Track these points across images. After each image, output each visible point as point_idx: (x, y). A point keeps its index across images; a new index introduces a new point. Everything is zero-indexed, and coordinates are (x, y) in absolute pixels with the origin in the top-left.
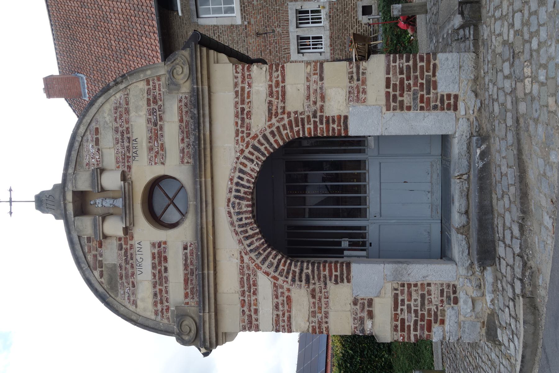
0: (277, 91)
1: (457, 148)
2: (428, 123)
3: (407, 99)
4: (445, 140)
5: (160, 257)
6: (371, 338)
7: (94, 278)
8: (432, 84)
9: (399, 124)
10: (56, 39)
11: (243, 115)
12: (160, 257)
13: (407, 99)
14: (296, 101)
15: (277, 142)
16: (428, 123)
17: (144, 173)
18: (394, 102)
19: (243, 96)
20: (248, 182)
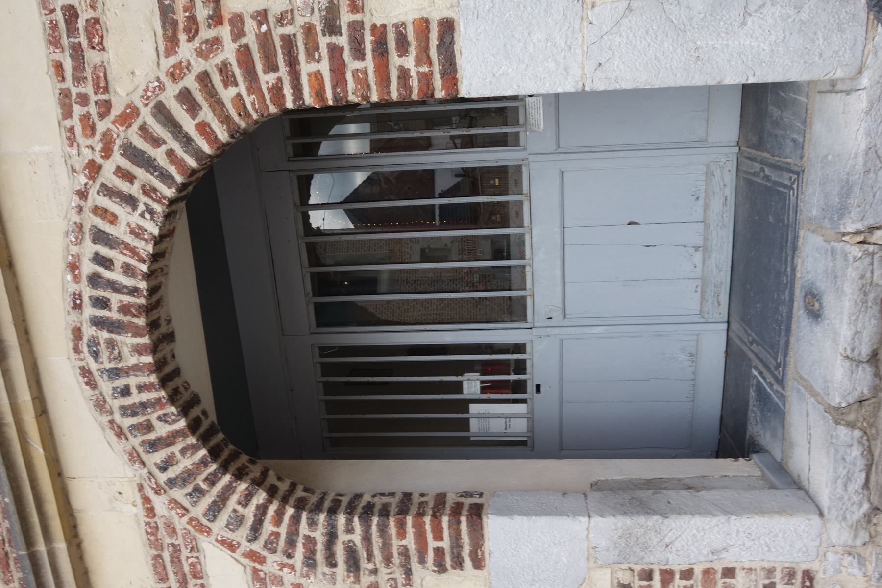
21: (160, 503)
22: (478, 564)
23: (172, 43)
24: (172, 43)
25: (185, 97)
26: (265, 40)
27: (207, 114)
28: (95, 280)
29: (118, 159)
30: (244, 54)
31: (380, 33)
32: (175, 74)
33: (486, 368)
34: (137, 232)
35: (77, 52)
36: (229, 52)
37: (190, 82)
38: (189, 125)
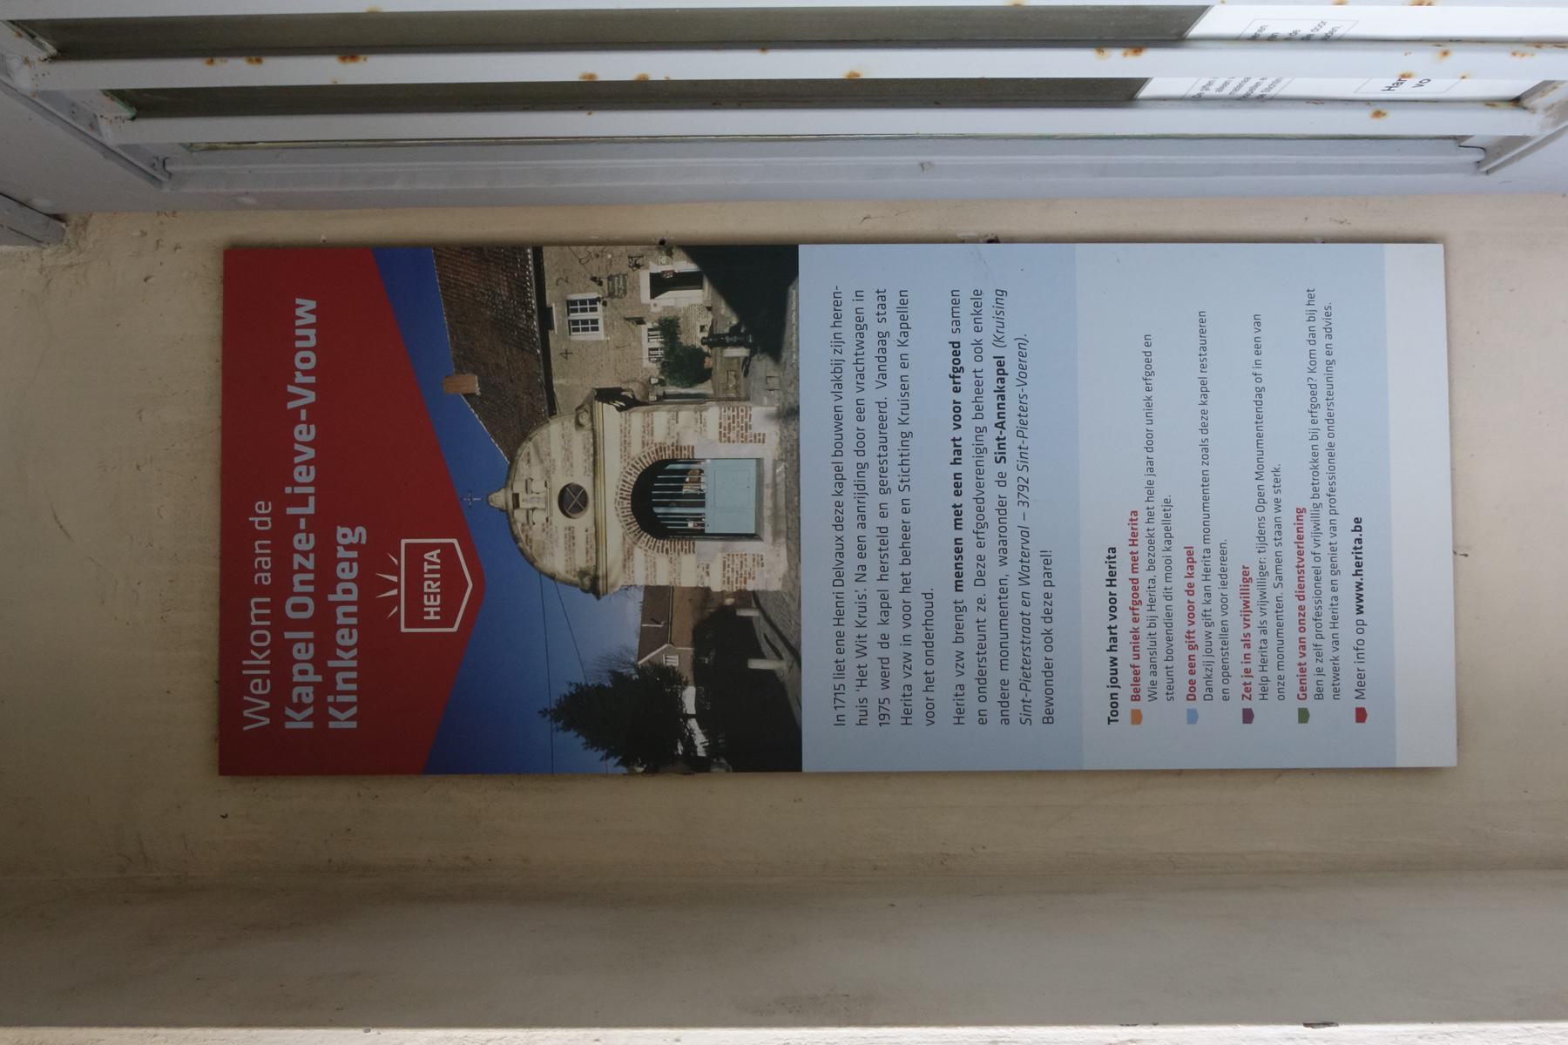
0: (648, 429)
1: (768, 465)
2: (748, 450)
3: (733, 435)
4: (759, 461)
5: (571, 535)
6: (708, 589)
7: (1459, 57)
8: (748, 427)
9: (725, 450)
10: (225, 17)
11: (626, 444)
12: (571, 535)
13: (733, 435)
14: (659, 436)
15: (648, 462)
16: (748, 450)
17: (559, 482)
18: (724, 437)
19: (625, 433)
20: (629, 488)
33: (681, 496)
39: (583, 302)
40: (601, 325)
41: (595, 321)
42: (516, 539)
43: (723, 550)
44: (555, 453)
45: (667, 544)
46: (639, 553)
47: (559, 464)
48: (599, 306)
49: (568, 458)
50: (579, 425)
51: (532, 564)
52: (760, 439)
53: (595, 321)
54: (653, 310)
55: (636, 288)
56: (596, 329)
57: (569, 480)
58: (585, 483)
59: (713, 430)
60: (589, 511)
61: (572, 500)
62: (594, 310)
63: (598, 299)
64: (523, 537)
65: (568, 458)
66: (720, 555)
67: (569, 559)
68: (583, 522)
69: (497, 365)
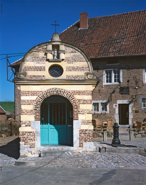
0: (85, 102)
8: (86, 141)
11: (79, 93)
13: (83, 135)
14: (82, 107)
15: (72, 102)
17: (63, 65)
19: (83, 93)
20: (61, 94)
21: (41, 93)
22: (35, 120)
23: (78, 100)
24: (78, 100)
25: (74, 100)
26: (78, 107)
27: (73, 102)
28: (61, 91)
29: (70, 94)
30: (77, 105)
31: (78, 115)
32: (76, 100)
34: (65, 95)
35: (78, 93)
36: (77, 104)
37: (75, 101)
38: (72, 100)
39: (119, 76)
40: (109, 84)
41: (110, 82)
42: (39, 45)
43: (37, 132)
44: (74, 63)
45: (39, 109)
46: (34, 98)
47: (71, 65)
48: (117, 83)
49: (74, 69)
50: (87, 74)
51: (29, 52)
52: (81, 145)
53: (110, 82)
54: (114, 105)
55: (123, 98)
56: (107, 82)
57: (65, 69)
58: (64, 76)
59: (85, 127)
60: (52, 78)
61: (56, 70)
62: (115, 81)
63: (120, 83)
64: (40, 48)
65: (74, 69)
66: (34, 130)
67: (31, 69)
68: (46, 74)
69: (92, 38)
